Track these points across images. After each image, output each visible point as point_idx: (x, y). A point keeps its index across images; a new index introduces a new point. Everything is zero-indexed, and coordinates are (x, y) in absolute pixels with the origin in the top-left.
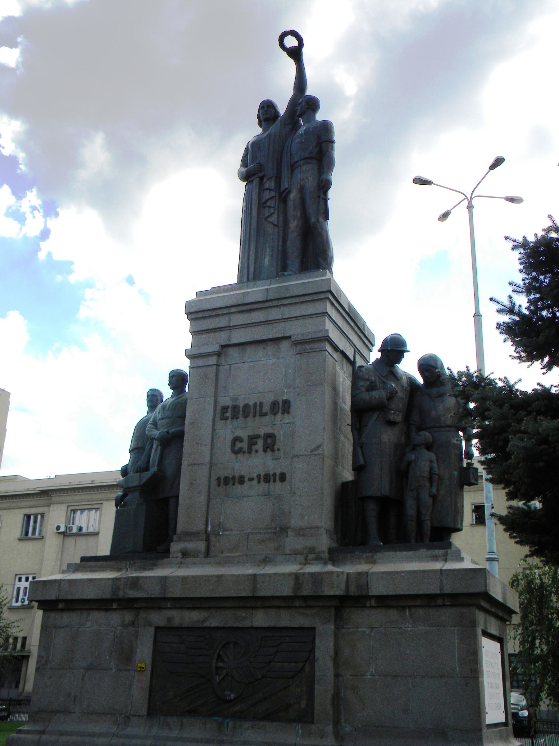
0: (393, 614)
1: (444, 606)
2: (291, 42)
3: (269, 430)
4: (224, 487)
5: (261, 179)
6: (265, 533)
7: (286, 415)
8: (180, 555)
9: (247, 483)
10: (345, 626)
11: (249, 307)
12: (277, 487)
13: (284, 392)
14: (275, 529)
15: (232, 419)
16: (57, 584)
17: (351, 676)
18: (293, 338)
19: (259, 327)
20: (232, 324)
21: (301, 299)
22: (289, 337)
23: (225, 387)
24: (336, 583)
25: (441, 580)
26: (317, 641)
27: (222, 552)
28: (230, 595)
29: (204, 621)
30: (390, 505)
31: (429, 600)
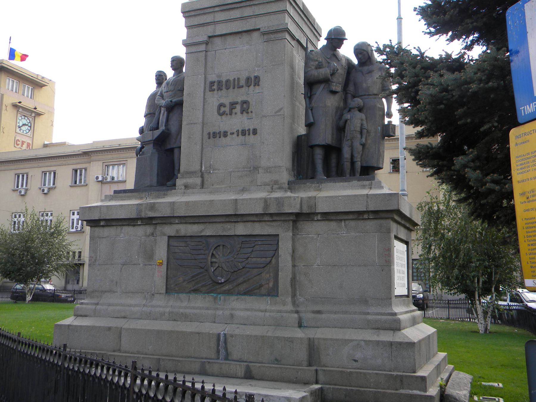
0: (333, 224)
3: (245, 98)
4: (213, 139)
7: (257, 87)
8: (183, 187)
11: (228, 7)
12: (251, 139)
14: (250, 168)
18: (262, 30)
19: (236, 22)
22: (259, 29)
25: (367, 202)
29: (201, 232)
30: (332, 151)
31: (359, 215)
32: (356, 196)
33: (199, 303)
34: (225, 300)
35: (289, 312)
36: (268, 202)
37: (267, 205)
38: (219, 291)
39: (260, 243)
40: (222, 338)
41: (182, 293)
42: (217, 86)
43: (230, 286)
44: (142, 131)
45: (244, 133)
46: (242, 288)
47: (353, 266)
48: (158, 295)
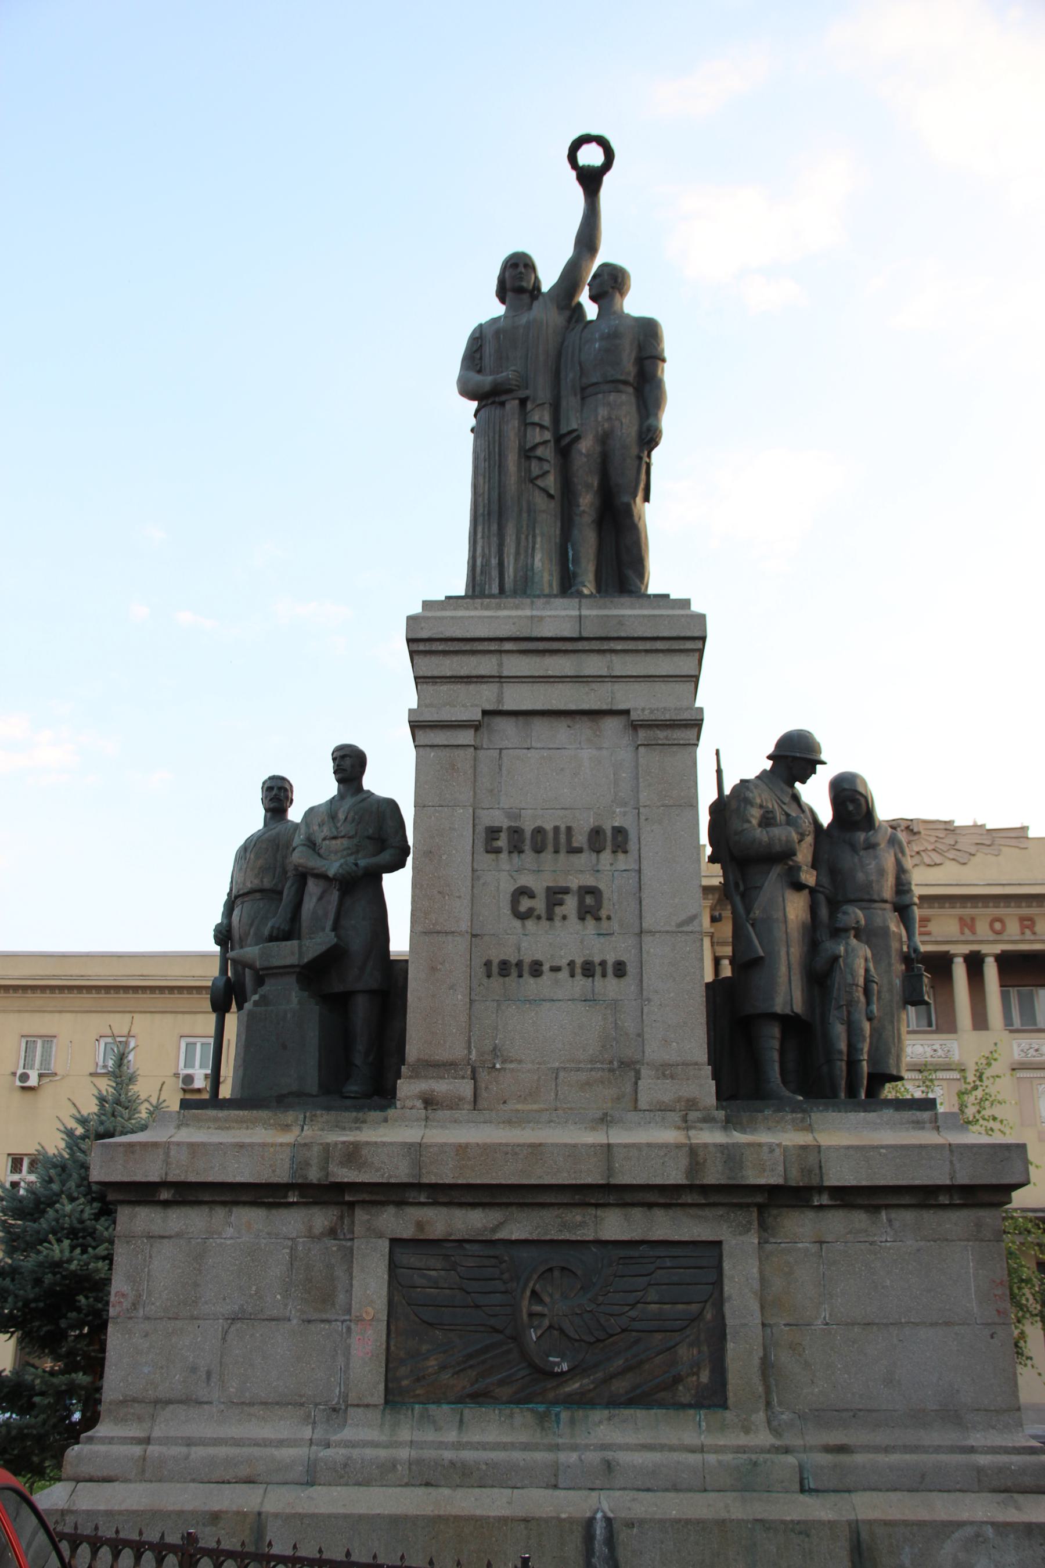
0: (859, 1219)
1: (951, 1206)
2: (591, 156)
3: (589, 881)
4: (501, 980)
5: (523, 402)
6: (592, 1070)
7: (621, 856)
8: (419, 1104)
9: (547, 977)
10: (772, 1240)
11: (541, 645)
12: (610, 987)
13: (614, 812)
14: (611, 1062)
15: (510, 852)
16: (161, 1151)
17: (785, 1325)
18: (634, 716)
19: (560, 685)
20: (505, 674)
21: (648, 645)
22: (626, 712)
23: (492, 791)
24: (768, 1163)
25: (951, 1162)
26: (726, 1266)
27: (505, 1102)
28: (560, 1182)
29: (494, 1230)
30: (802, 1032)
31: (925, 1197)
32: (921, 1147)
33: (494, 1435)
34: (572, 1422)
35: (769, 1452)
36: (701, 1153)
37: (698, 1163)
38: (551, 1395)
39: (669, 1264)
40: (599, 1530)
41: (438, 1402)
42: (506, 840)
43: (585, 1381)
44: (223, 936)
45: (588, 970)
46: (620, 1386)
47: (916, 1324)
48: (360, 1410)
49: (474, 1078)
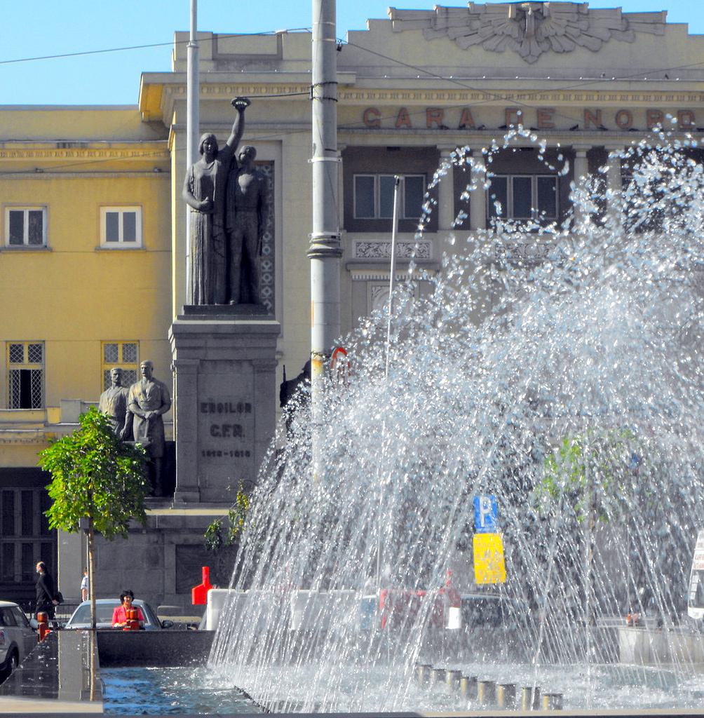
42: (209, 407)
45: (237, 454)
49: (199, 491)
